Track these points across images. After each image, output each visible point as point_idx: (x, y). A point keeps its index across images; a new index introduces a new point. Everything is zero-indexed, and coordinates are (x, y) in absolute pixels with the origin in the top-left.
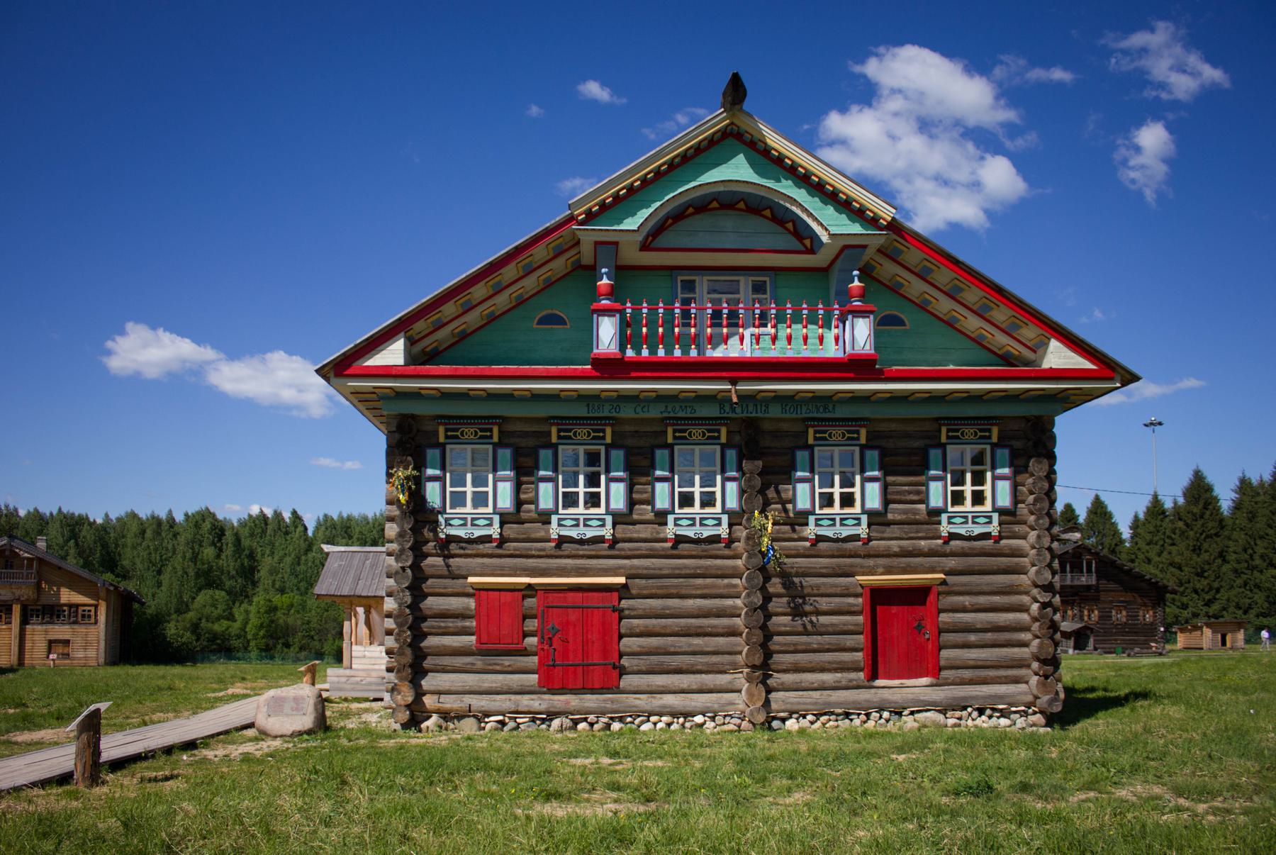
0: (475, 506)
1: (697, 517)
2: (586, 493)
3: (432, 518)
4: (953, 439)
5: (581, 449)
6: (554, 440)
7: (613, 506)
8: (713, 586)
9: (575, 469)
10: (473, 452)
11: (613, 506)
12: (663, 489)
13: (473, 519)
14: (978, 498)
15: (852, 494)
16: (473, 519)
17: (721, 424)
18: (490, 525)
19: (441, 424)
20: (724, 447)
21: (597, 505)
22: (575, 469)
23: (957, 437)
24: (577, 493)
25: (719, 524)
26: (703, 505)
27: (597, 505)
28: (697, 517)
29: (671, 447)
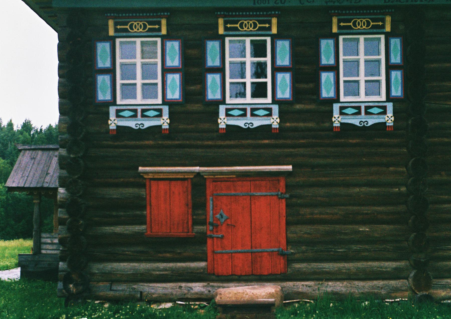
0: (144, 97)
1: (139, 109)
2: (252, 83)
3: (104, 109)
4: (123, 32)
5: (248, 40)
6: (335, 30)
7: (280, 95)
8: (167, 175)
9: (243, 59)
10: (142, 43)
11: (280, 95)
12: (214, 79)
13: (143, 111)
14: (259, 91)
15: (266, 83)
16: (367, 108)
17: (161, 17)
18: (160, 116)
19: (221, 16)
20: (388, 36)
21: (265, 95)
22: (243, 59)
23: (236, 29)
24: (357, 82)
25: (385, 113)
26: (254, 95)
27: (265, 95)
28: (139, 109)
29: (112, 40)
